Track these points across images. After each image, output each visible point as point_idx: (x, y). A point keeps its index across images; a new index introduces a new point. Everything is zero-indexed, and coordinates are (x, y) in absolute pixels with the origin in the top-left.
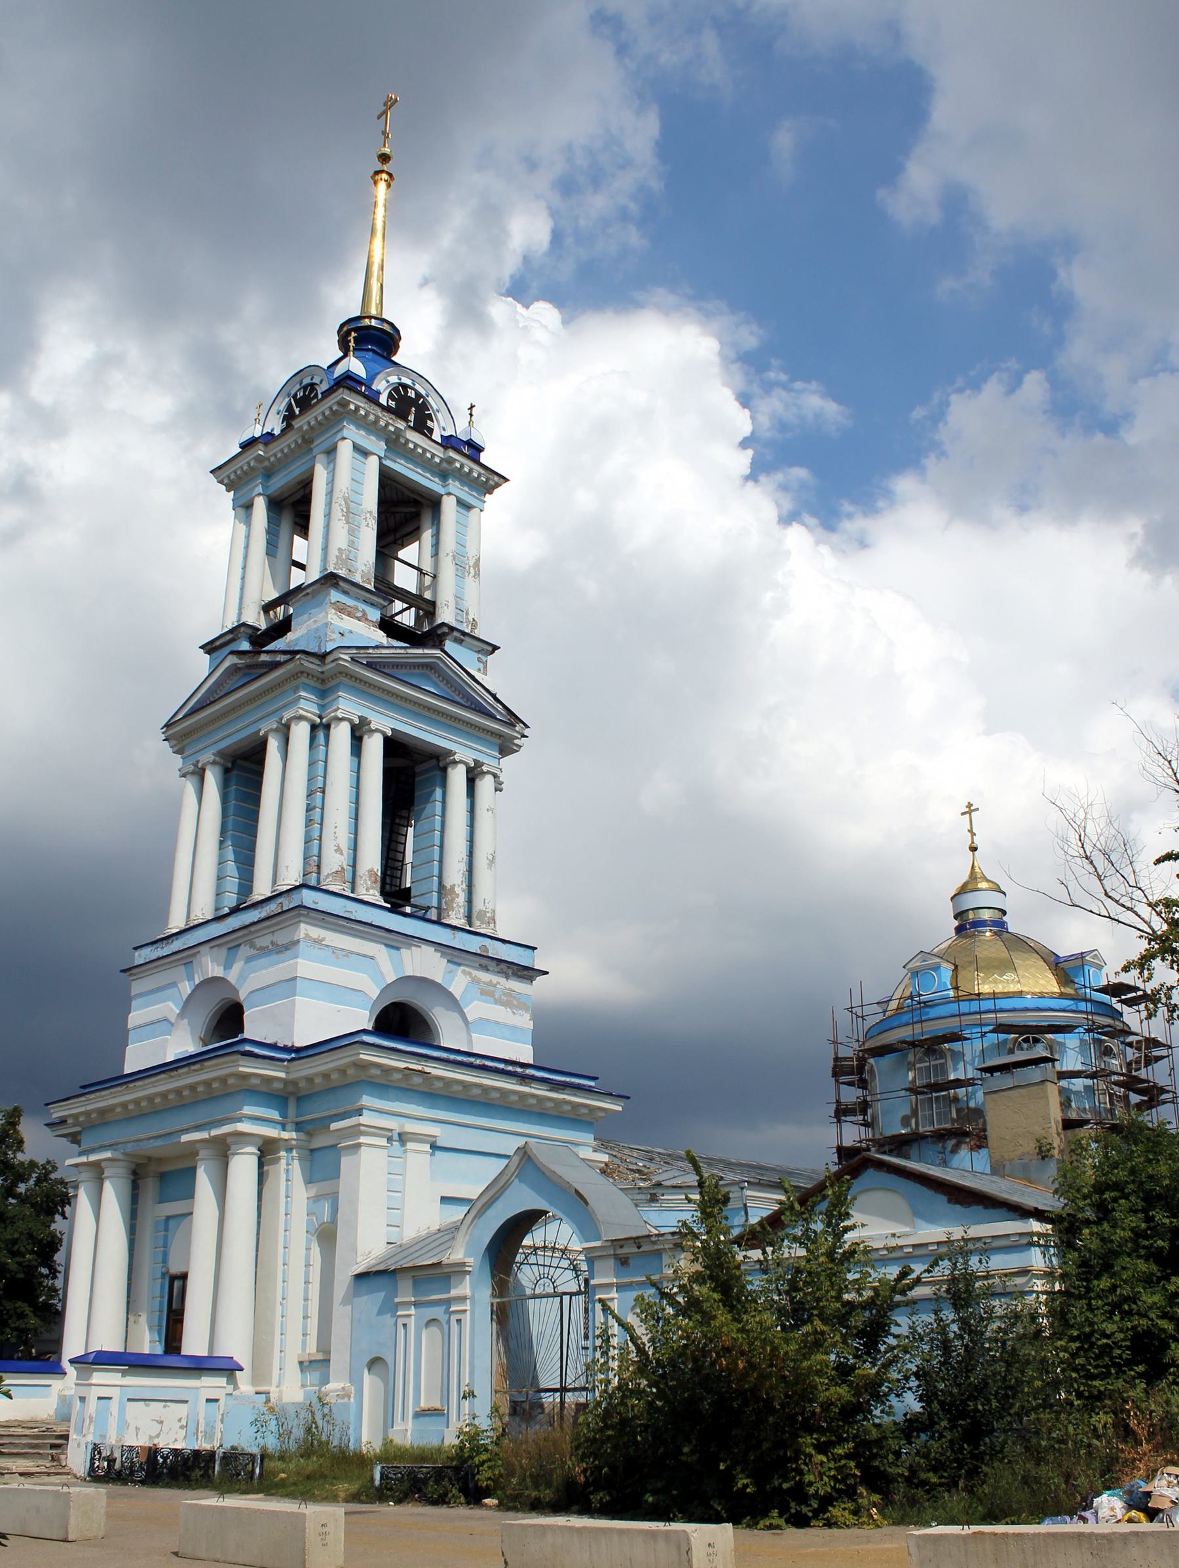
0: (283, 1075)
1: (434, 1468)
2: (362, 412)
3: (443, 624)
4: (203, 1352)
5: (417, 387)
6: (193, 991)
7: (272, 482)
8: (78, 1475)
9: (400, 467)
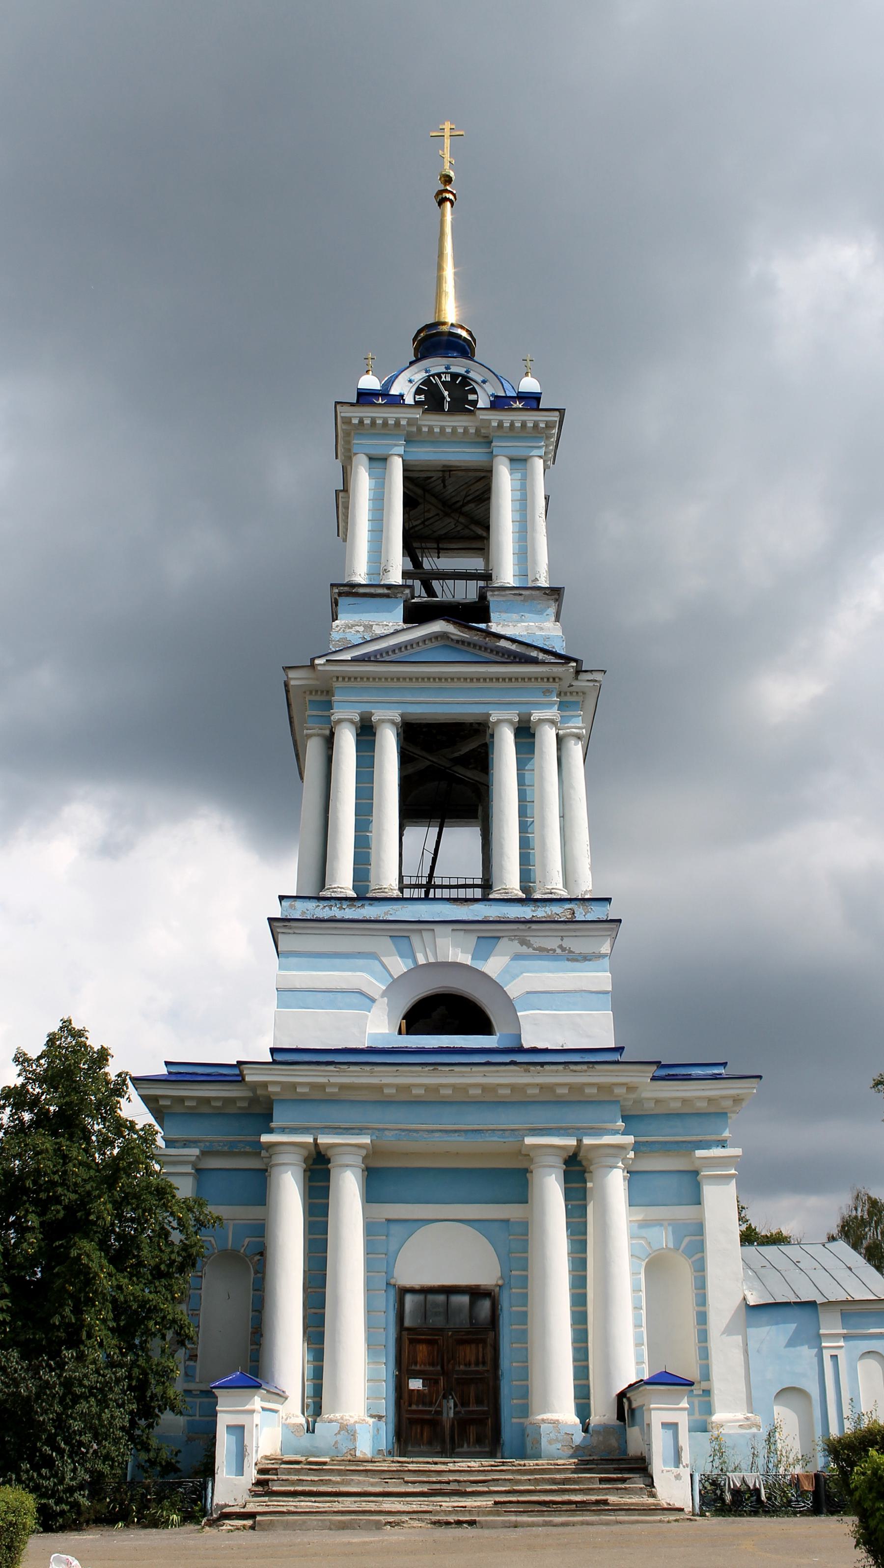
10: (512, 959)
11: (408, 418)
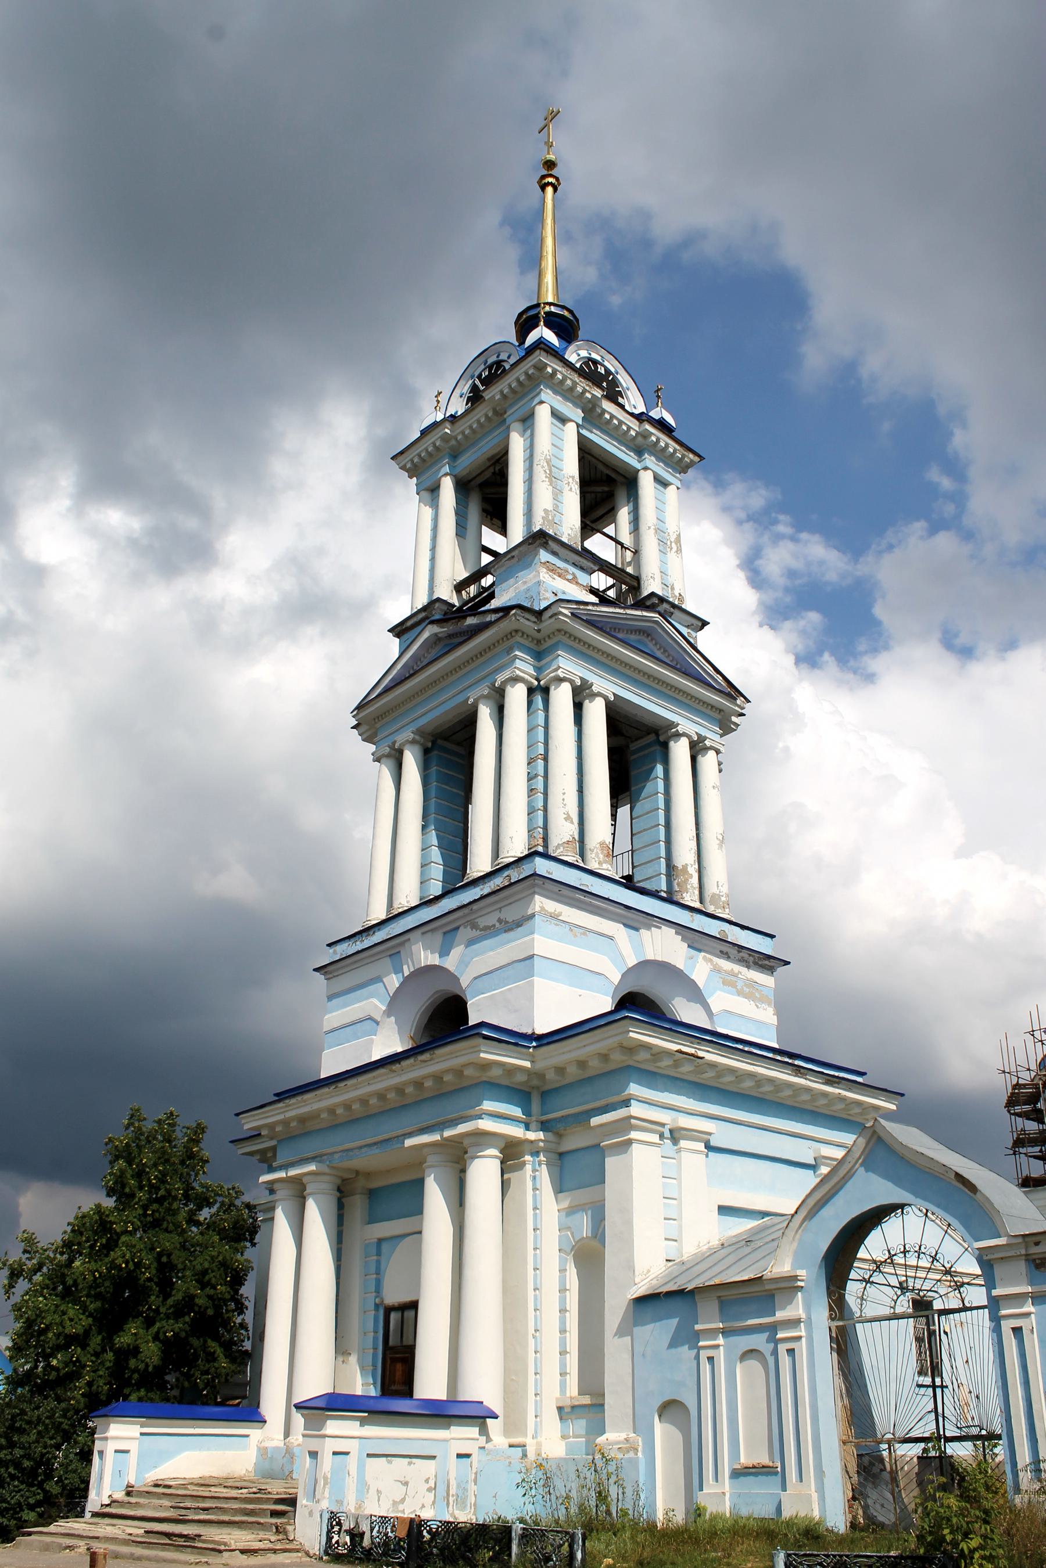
0: (527, 1064)
1: (880, 1557)
2: (560, 376)
3: (653, 594)
4: (441, 1394)
5: (606, 363)
6: (402, 985)
7: (458, 462)
8: (311, 1552)
9: (596, 437)
10: (466, 947)
11: (439, 438)
